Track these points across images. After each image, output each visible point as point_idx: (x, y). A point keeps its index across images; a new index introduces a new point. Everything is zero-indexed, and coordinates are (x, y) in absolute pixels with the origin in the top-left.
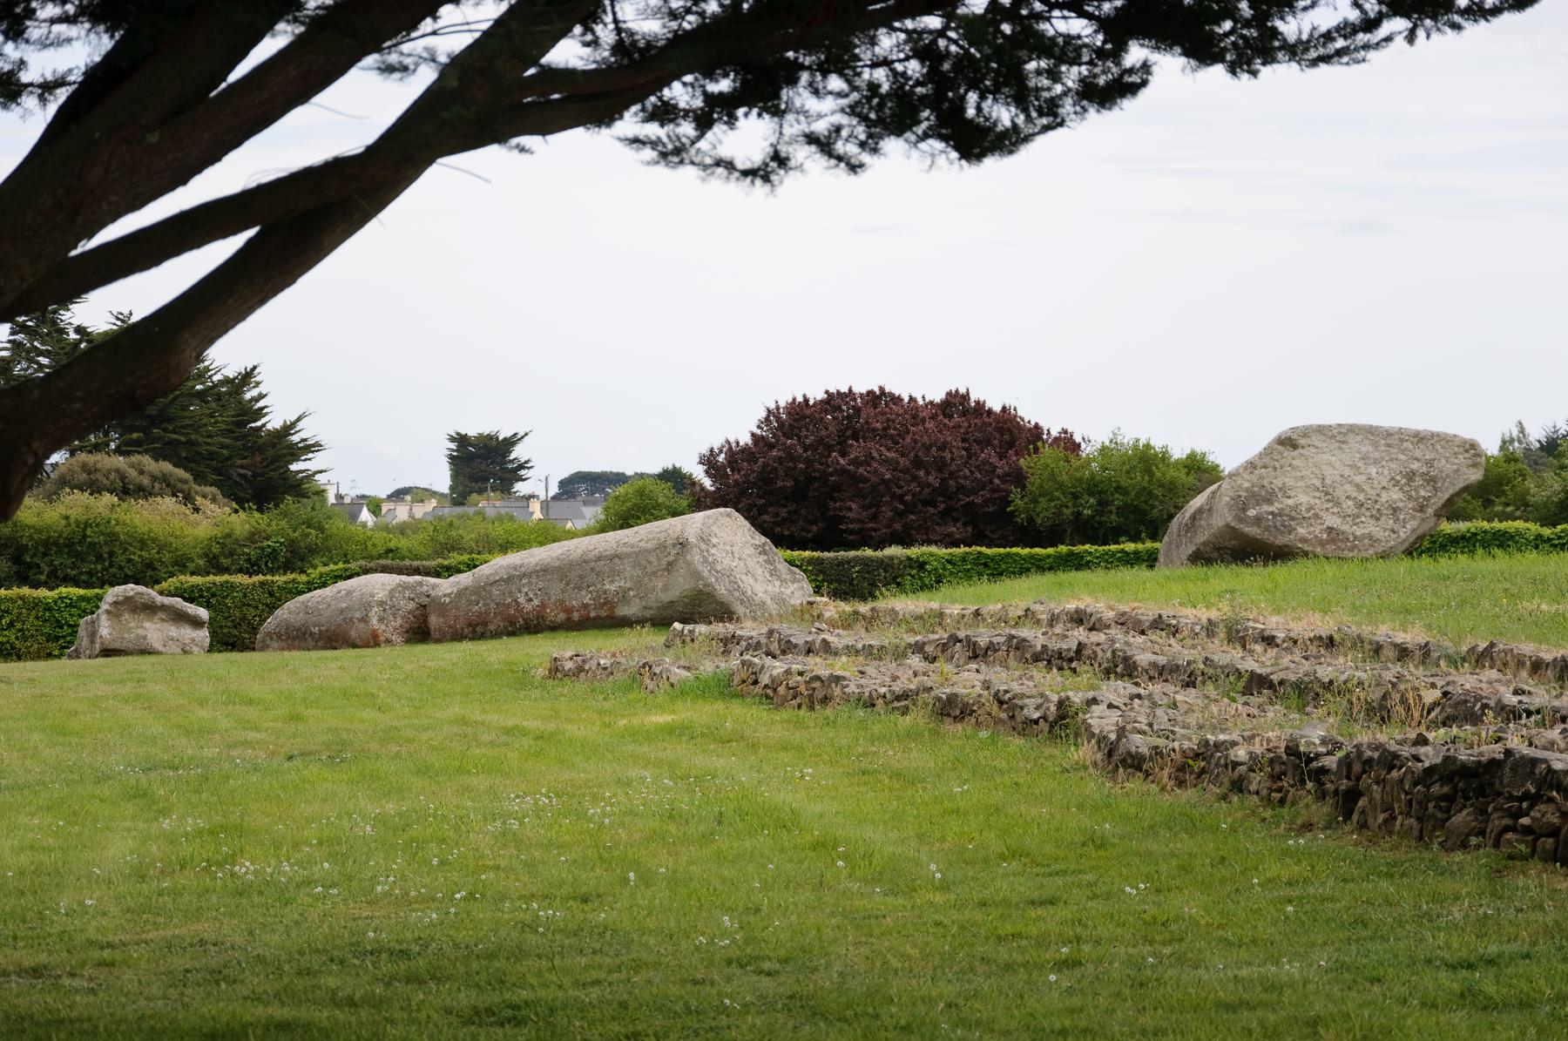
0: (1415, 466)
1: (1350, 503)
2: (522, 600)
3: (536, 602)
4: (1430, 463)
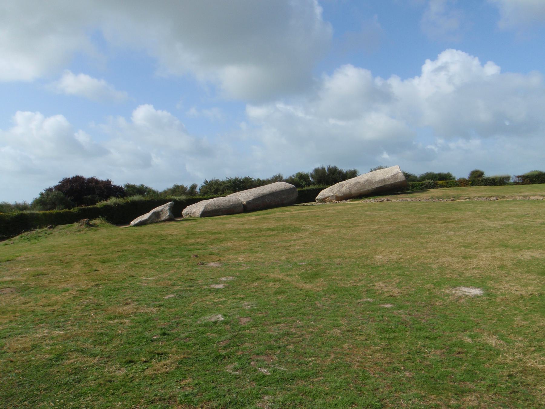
2: (267, 201)
3: (269, 201)
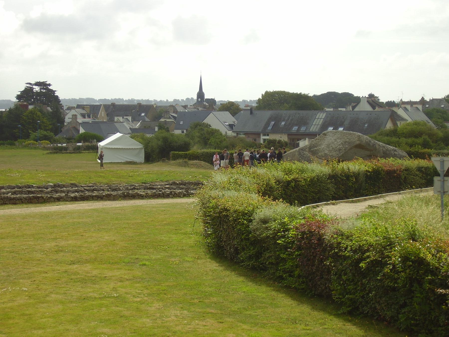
0: (347, 140)
1: (331, 148)
4: (350, 139)
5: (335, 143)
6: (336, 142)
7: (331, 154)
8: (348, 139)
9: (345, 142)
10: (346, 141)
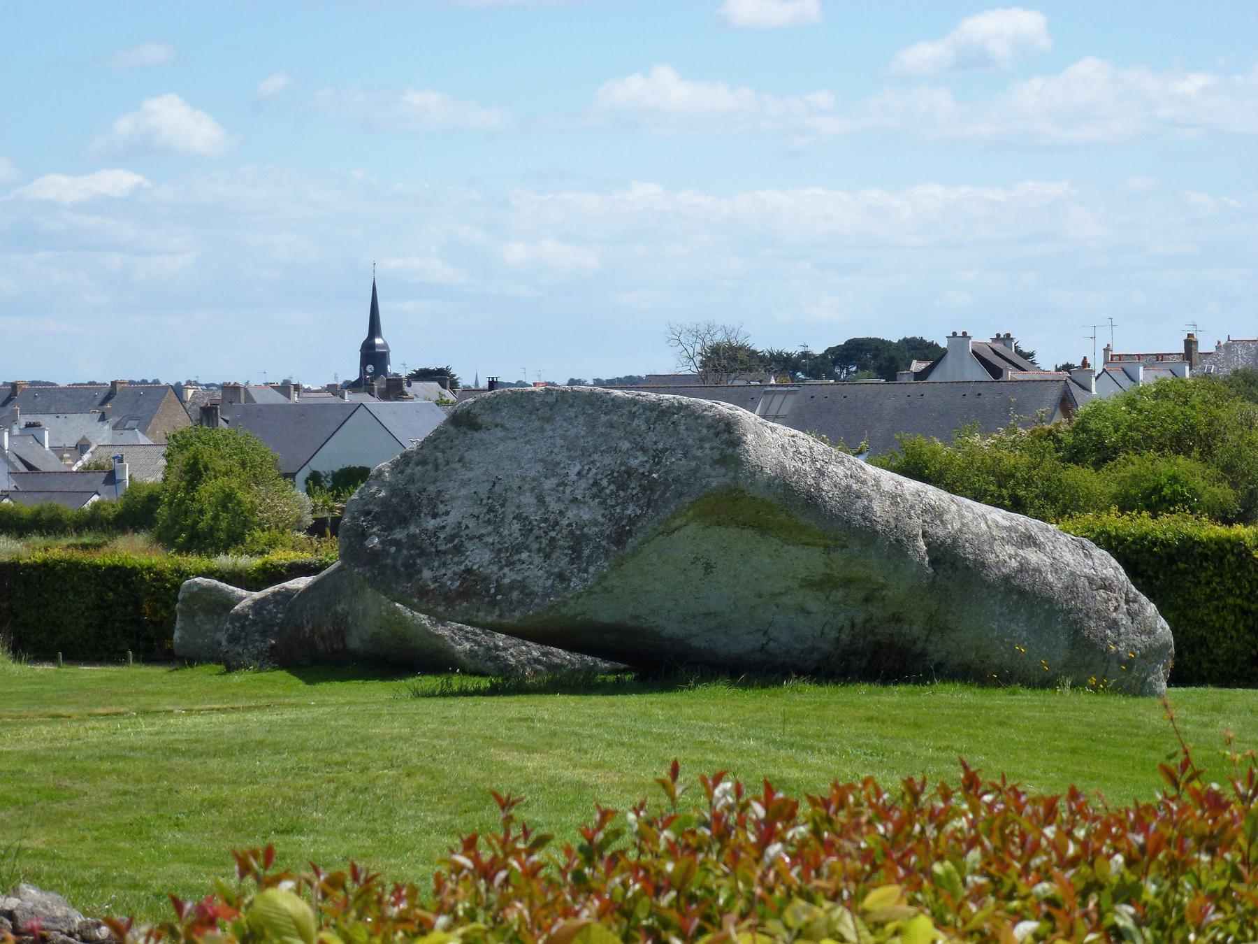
5: (549, 484)
6: (554, 481)
7: (509, 576)
8: (644, 450)
9: (622, 478)
10: (629, 473)
